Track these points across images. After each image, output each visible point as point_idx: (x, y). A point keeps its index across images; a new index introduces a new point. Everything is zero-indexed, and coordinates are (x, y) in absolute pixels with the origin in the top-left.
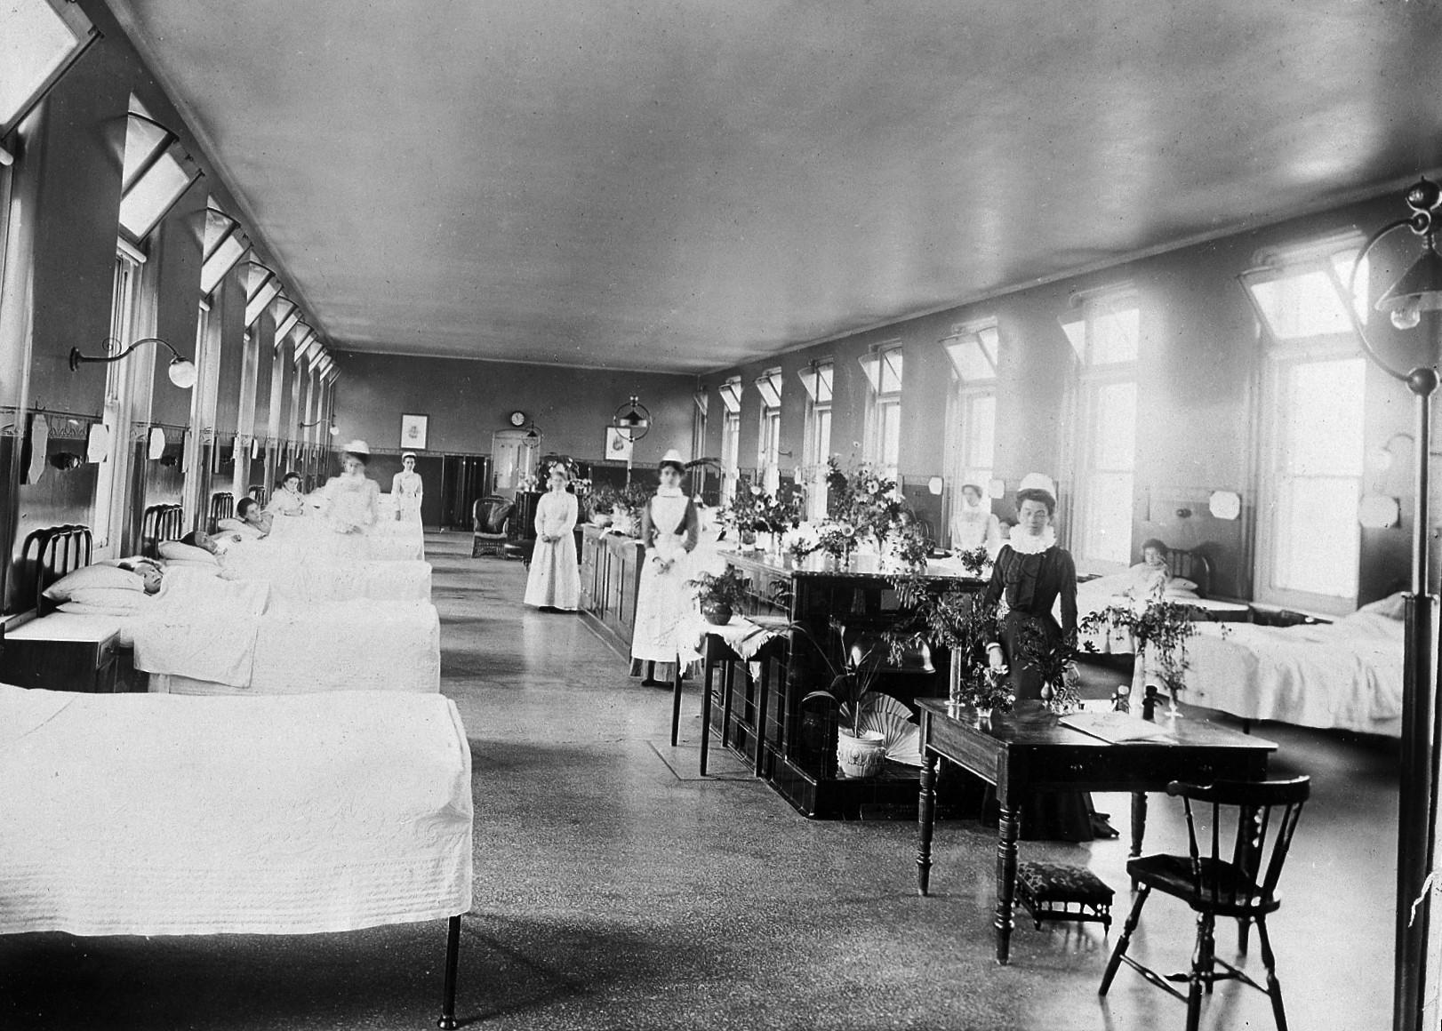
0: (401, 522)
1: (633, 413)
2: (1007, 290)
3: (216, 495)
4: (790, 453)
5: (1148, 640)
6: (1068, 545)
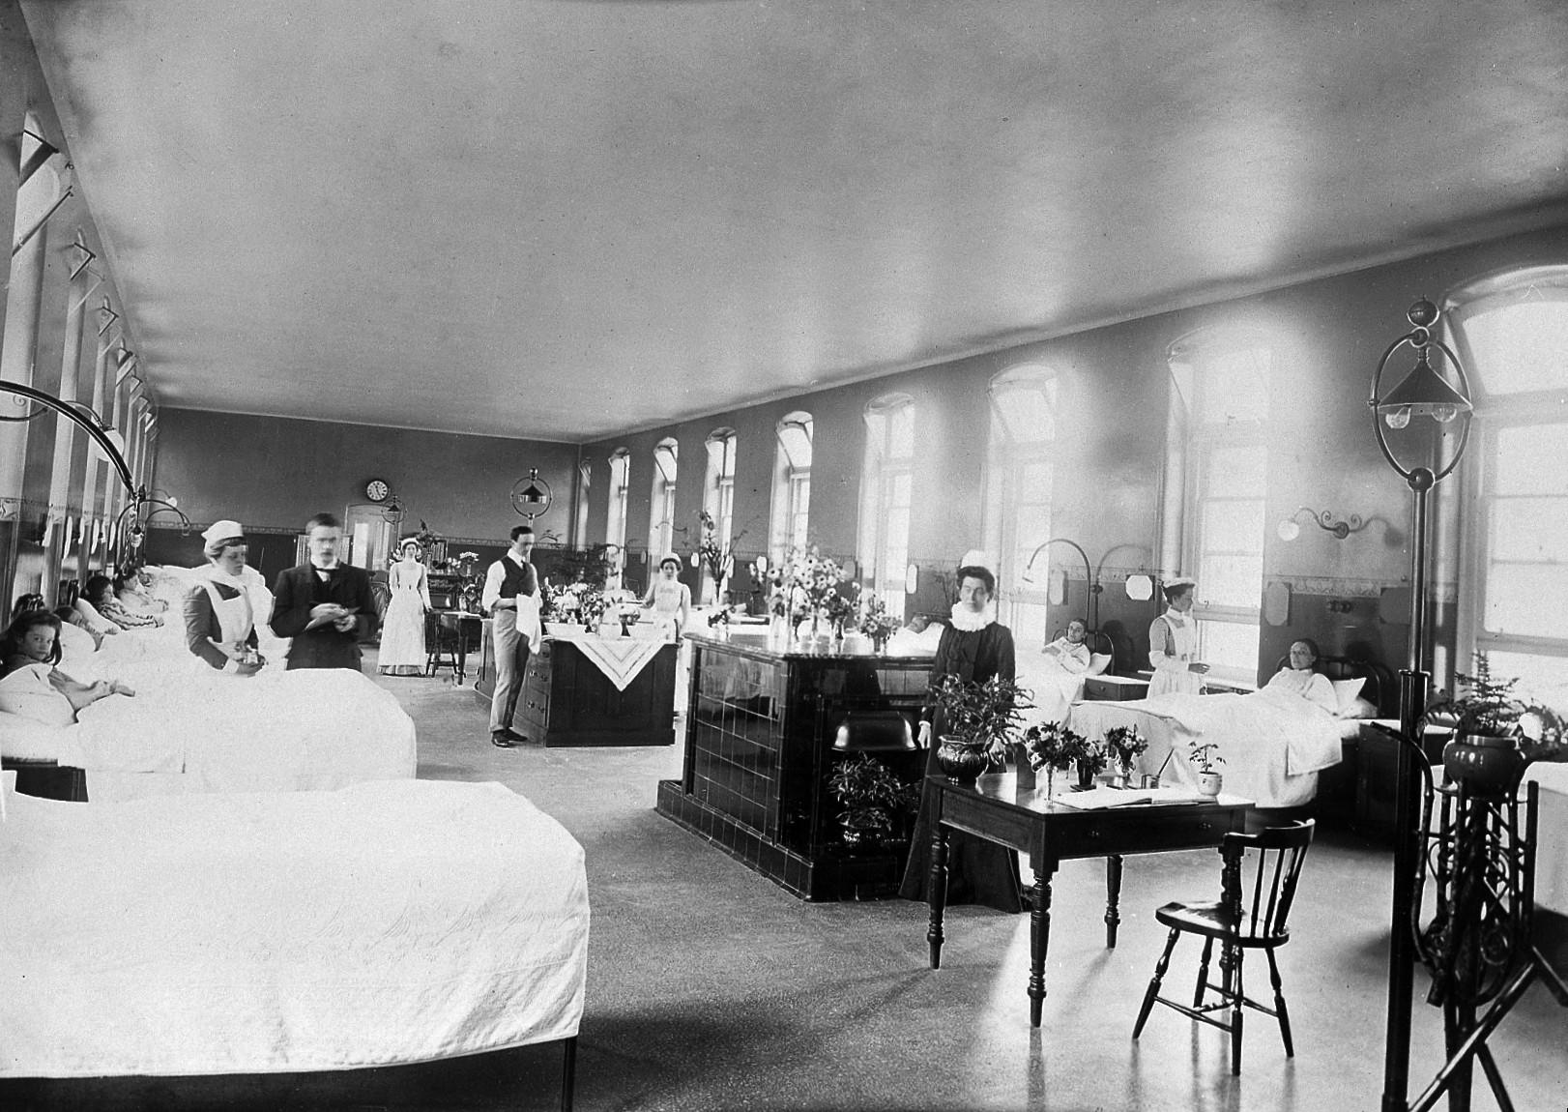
1: (532, 488)
4: (686, 529)
6: (1009, 619)
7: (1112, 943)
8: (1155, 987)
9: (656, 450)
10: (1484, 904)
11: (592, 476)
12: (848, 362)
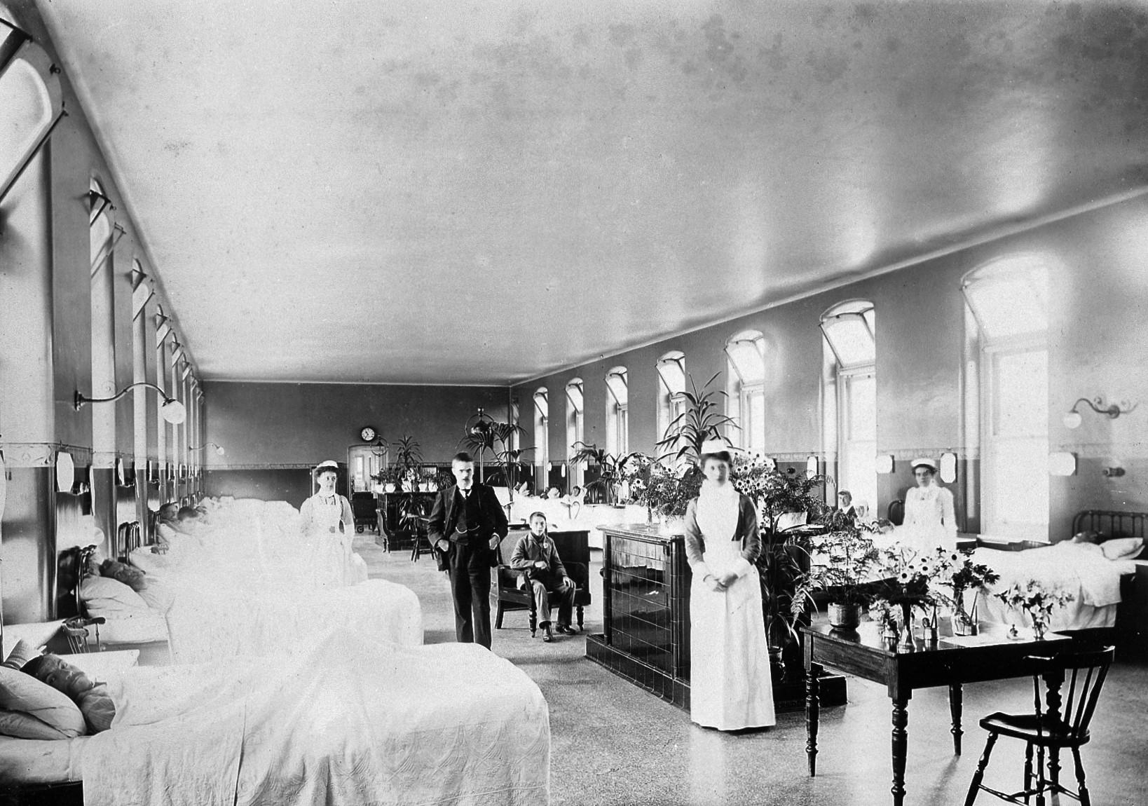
0: (12, 481)
7: (958, 751)
8: (978, 777)
9: (660, 363)
11: (520, 410)
12: (714, 313)
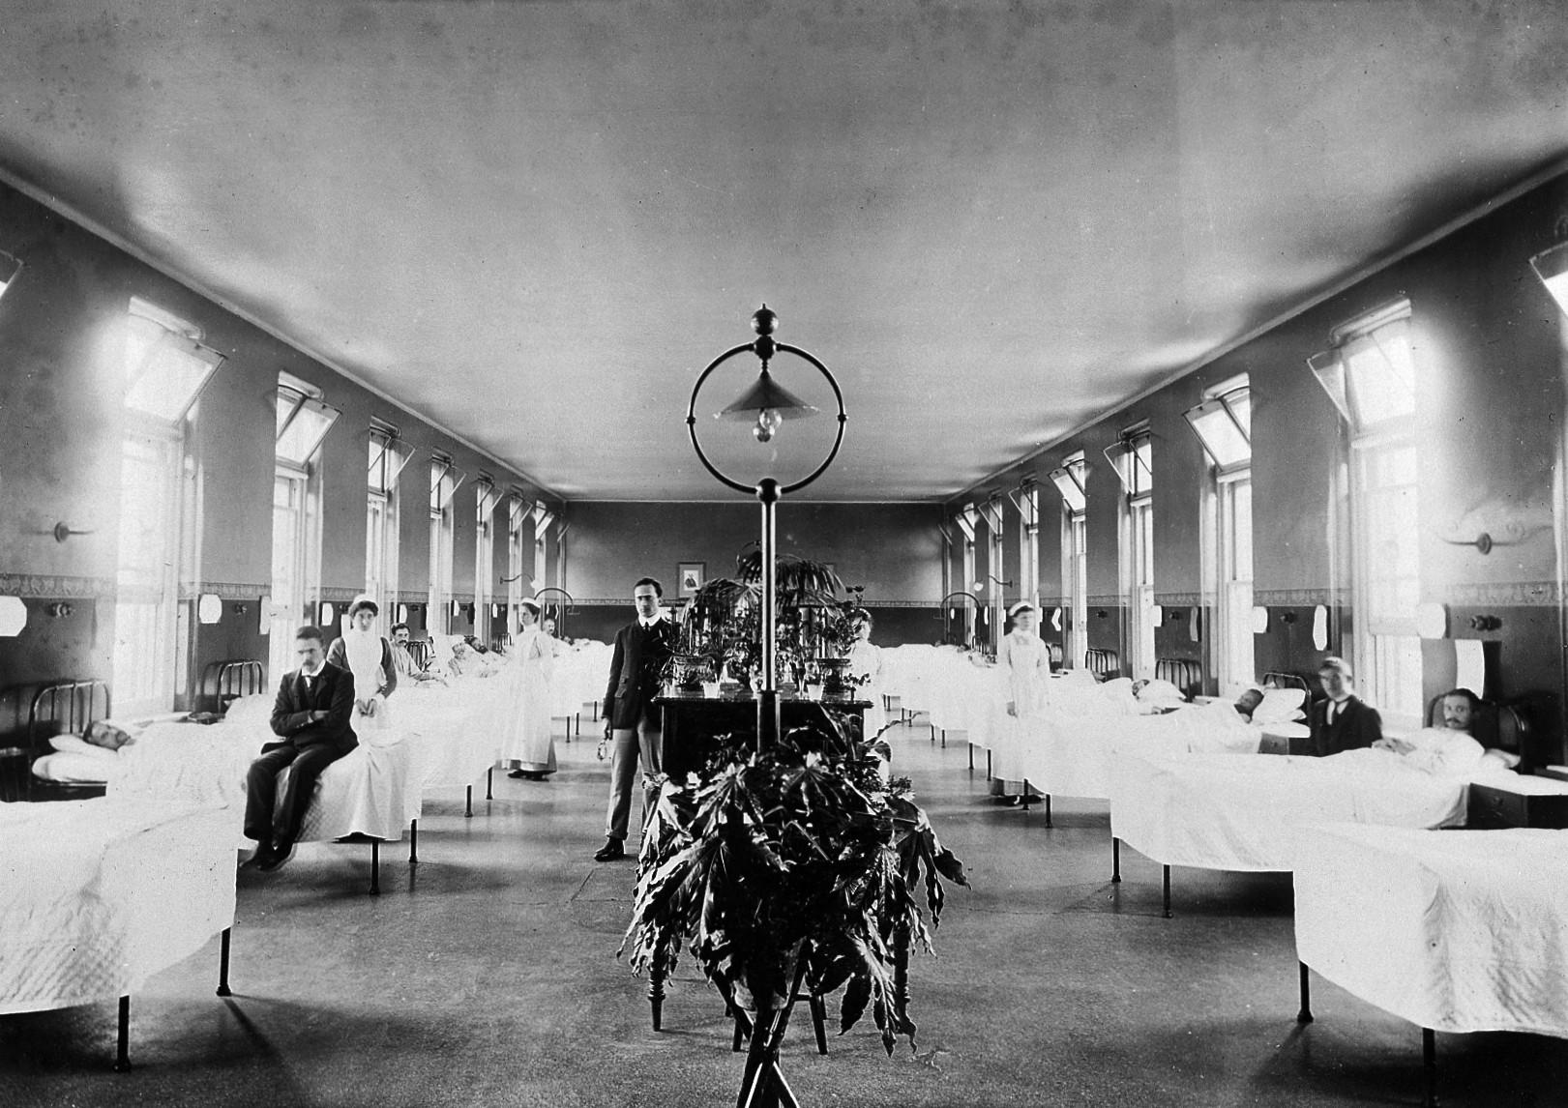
2: (1246, 338)
3: (729, 676)
5: (38, 767)
10: (761, 1065)
